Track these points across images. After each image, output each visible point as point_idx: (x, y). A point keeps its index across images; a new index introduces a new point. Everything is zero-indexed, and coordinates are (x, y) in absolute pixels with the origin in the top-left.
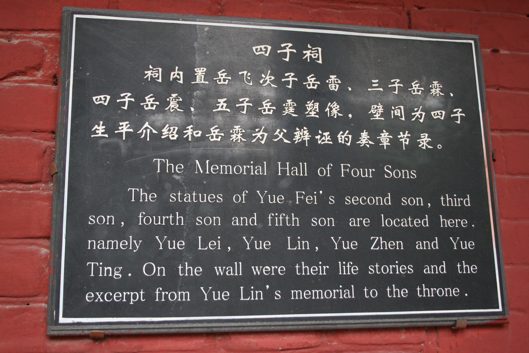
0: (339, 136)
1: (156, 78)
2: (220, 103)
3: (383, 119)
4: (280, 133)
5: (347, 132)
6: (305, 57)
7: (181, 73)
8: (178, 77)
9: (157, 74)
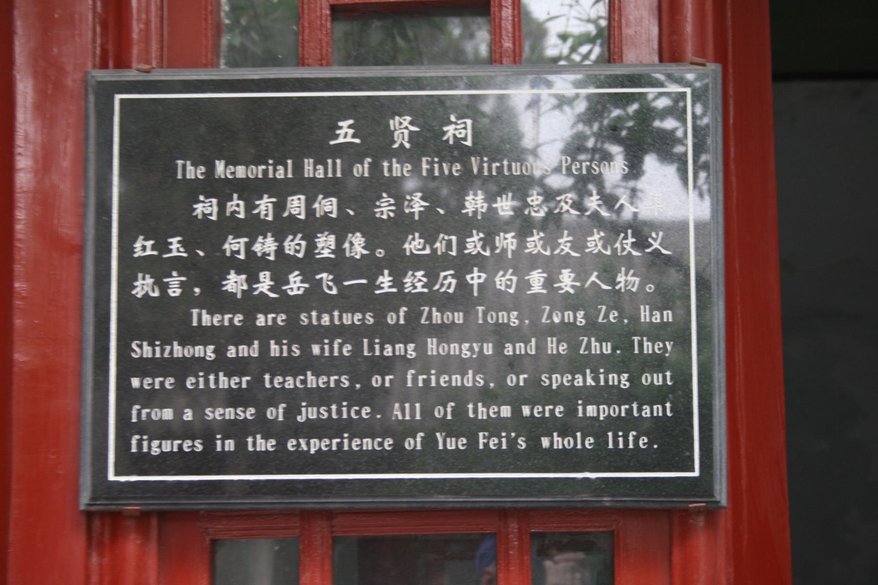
0: (497, 279)
1: (462, 139)
2: (341, 128)
5: (511, 271)
7: (241, 203)
8: (237, 209)
9: (463, 131)
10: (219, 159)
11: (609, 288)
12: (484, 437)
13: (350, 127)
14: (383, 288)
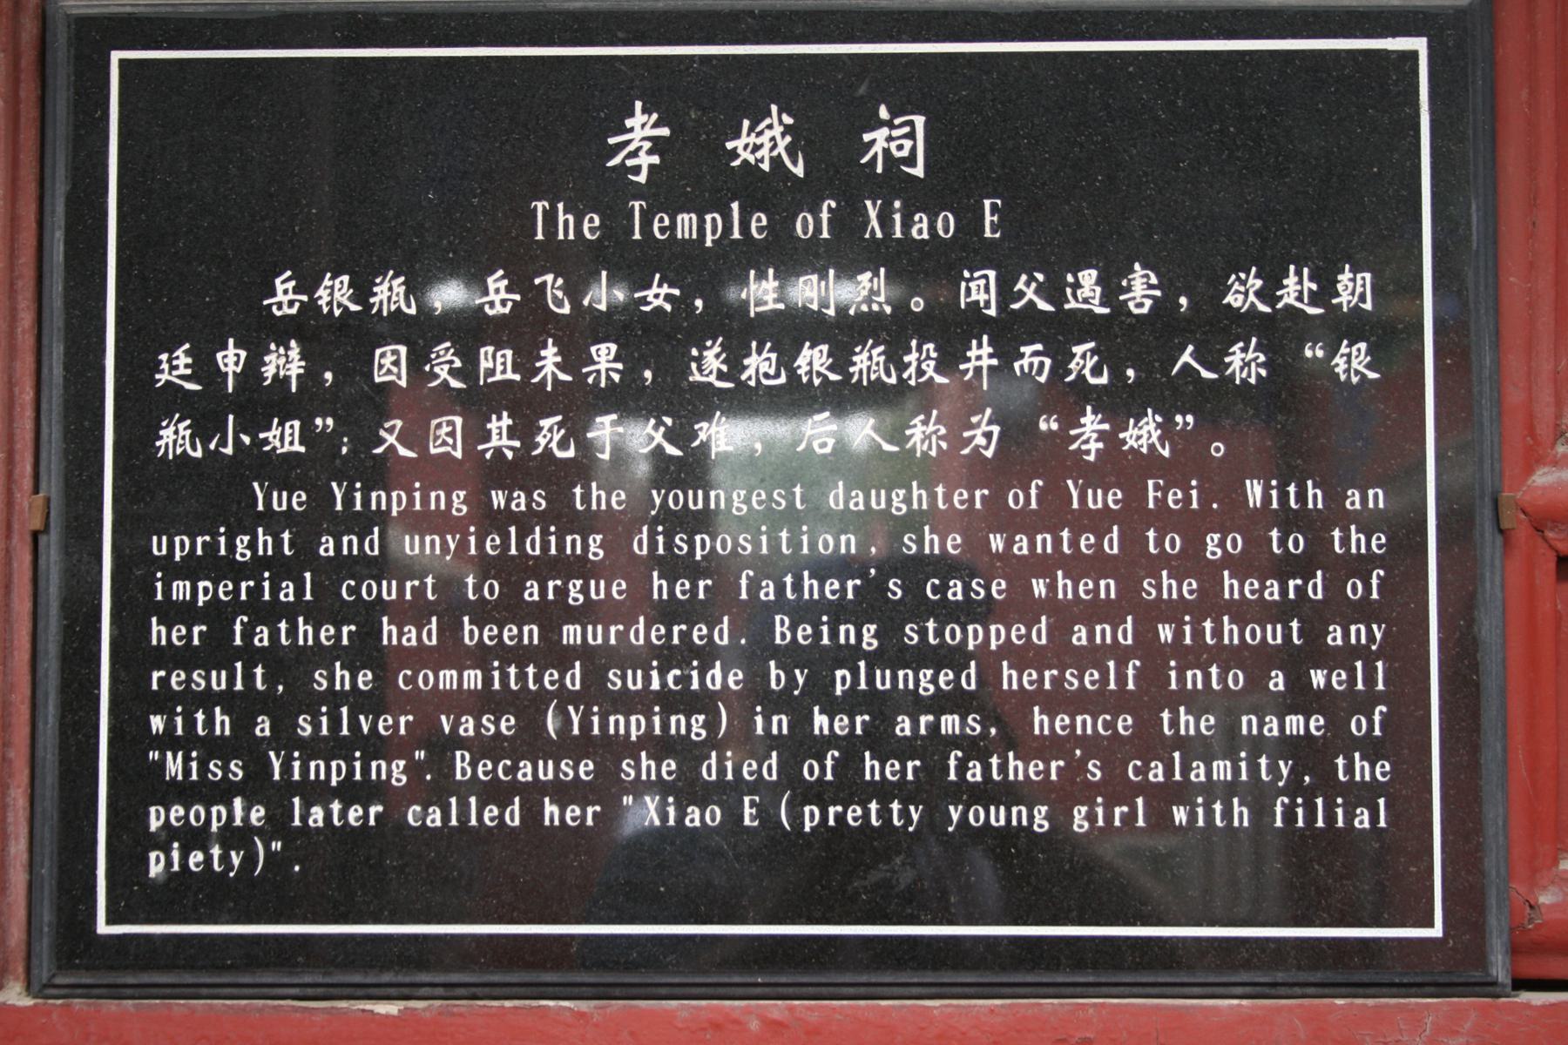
4: (1028, 284)
6: (871, 153)
9: (908, 144)
10: (1178, 806)
11: (896, 449)
12: (1157, 487)
14: (766, 303)
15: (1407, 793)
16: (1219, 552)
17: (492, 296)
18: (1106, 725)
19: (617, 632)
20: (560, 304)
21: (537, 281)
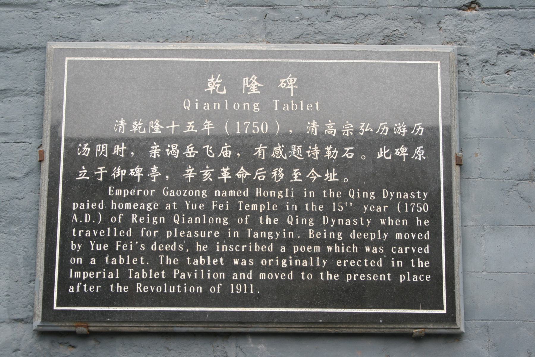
2: (189, 125)
3: (88, 178)
13: (192, 124)
15: (435, 270)
16: (151, 209)
17: (188, 152)
18: (422, 278)
19: (210, 233)
20: (211, 154)
21: (204, 147)
